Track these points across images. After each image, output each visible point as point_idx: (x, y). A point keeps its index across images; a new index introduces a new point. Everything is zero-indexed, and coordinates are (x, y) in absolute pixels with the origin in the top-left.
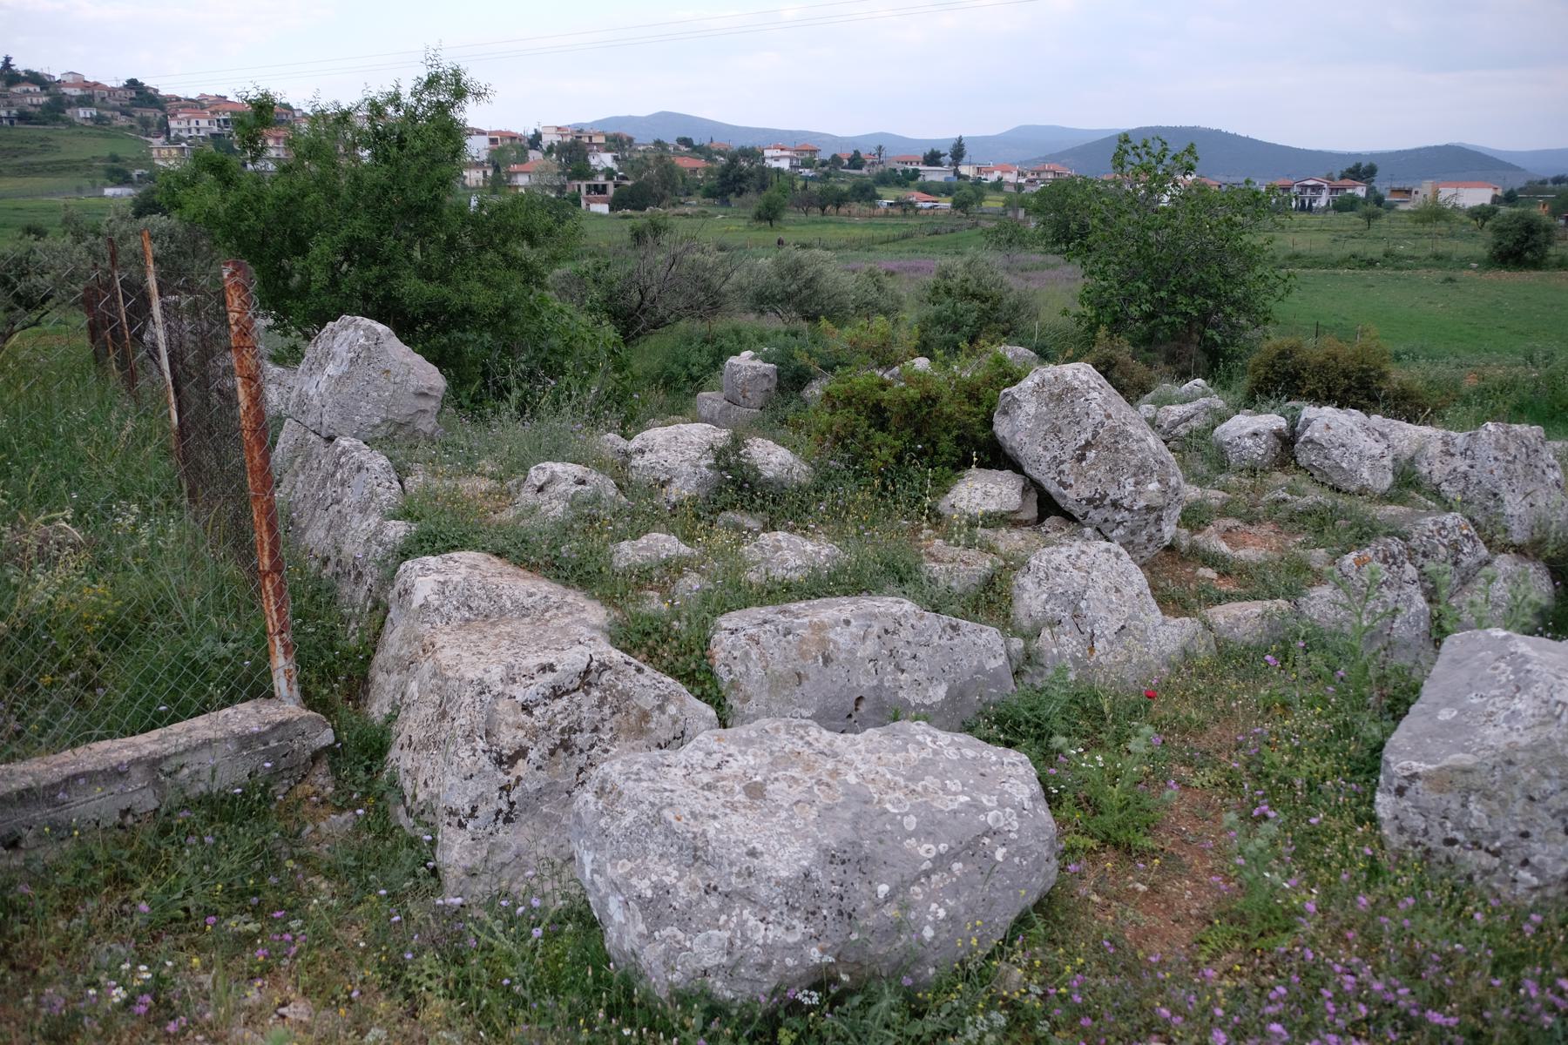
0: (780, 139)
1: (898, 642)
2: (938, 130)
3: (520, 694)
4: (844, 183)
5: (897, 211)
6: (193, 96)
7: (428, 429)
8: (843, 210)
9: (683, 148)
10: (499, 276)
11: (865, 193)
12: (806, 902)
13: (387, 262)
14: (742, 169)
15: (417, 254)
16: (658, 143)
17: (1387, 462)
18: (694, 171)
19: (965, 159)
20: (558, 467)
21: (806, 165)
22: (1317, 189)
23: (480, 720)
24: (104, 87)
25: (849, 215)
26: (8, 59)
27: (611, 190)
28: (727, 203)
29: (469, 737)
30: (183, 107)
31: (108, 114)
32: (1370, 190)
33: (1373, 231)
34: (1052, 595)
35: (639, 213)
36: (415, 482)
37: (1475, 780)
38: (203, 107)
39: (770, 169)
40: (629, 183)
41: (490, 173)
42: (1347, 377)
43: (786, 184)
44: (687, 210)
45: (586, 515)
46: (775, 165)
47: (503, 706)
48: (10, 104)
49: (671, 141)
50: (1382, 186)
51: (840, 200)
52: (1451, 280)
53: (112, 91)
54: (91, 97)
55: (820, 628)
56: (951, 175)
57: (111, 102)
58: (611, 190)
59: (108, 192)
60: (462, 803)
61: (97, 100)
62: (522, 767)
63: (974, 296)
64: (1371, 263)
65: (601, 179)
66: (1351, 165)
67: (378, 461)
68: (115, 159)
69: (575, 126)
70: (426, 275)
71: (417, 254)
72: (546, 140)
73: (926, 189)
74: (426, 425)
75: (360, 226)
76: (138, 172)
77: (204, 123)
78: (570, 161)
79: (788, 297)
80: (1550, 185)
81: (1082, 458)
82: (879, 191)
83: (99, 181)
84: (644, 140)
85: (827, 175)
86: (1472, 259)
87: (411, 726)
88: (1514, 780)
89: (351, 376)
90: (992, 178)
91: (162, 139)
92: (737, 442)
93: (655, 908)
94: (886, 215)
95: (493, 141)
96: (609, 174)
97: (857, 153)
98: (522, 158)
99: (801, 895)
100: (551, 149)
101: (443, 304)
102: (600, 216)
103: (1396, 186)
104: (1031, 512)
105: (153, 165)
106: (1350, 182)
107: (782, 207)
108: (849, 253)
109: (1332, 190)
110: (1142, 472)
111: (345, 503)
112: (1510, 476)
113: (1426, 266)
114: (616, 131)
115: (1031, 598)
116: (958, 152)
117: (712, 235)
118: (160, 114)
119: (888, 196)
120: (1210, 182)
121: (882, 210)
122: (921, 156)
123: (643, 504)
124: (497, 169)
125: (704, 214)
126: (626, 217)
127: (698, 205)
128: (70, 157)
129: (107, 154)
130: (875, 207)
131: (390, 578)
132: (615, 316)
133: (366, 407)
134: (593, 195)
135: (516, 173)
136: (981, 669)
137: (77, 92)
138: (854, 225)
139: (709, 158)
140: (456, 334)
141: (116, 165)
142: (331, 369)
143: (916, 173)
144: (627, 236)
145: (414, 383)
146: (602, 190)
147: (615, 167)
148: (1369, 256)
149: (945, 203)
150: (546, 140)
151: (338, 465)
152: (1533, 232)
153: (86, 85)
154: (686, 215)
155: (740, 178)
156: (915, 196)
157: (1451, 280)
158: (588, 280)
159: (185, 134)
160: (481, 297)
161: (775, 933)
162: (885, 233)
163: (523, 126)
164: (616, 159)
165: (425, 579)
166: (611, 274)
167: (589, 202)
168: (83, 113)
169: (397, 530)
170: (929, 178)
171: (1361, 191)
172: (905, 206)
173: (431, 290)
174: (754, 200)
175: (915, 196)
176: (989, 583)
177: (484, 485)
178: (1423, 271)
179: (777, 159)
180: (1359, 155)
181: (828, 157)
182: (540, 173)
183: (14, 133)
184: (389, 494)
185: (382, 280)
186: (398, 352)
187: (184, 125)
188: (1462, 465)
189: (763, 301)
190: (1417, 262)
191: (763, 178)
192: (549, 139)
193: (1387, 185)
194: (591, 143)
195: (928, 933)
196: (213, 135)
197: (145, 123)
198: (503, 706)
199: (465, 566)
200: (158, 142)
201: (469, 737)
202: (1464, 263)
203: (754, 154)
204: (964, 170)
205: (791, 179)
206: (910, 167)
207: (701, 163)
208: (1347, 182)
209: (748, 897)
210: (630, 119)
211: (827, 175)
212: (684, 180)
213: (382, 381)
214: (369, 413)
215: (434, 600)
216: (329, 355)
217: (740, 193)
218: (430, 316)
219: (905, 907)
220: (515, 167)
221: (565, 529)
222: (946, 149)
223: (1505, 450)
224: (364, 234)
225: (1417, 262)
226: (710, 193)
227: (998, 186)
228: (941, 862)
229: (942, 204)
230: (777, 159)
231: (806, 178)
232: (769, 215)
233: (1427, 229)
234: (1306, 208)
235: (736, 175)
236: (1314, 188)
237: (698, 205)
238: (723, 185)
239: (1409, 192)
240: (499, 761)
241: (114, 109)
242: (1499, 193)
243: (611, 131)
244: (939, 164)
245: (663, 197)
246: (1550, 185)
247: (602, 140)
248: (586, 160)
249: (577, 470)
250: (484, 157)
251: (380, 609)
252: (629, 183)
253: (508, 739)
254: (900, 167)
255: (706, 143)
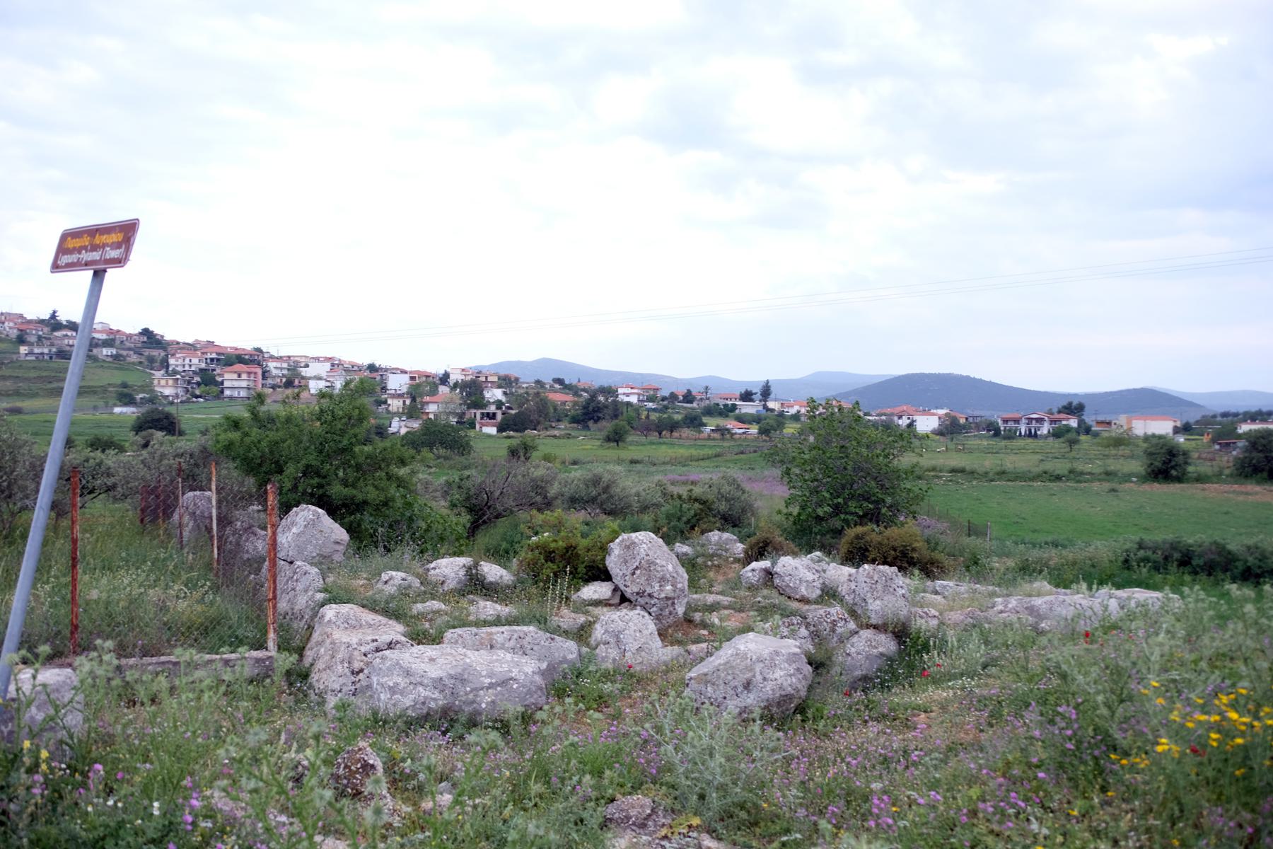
0: (630, 380)
1: (525, 642)
2: (753, 376)
3: (363, 649)
4: (677, 414)
5: (717, 435)
6: (190, 341)
7: (339, 559)
8: (675, 434)
9: (557, 386)
10: (383, 484)
11: (694, 422)
12: (440, 687)
13: (325, 477)
14: (599, 402)
15: (341, 474)
16: (538, 382)
17: (817, 584)
18: (564, 403)
19: (772, 396)
20: (394, 573)
21: (650, 399)
22: (1040, 420)
23: (347, 656)
24: (124, 334)
25: (680, 438)
26: (55, 312)
27: (499, 417)
28: (587, 428)
29: (342, 662)
30: (182, 348)
31: (124, 353)
32: (1081, 422)
33: (1073, 454)
34: (606, 631)
35: (519, 434)
36: (330, 579)
37: (709, 678)
38: (196, 349)
39: (622, 403)
40: (513, 412)
41: (408, 402)
42: (895, 550)
43: (633, 414)
44: (556, 432)
45: (404, 591)
46: (626, 399)
47: (356, 653)
48: (52, 345)
49: (547, 380)
50: (1089, 419)
51: (673, 427)
52: (1113, 490)
53: (130, 336)
54: (113, 340)
55: (491, 634)
56: (761, 408)
57: (128, 344)
58: (499, 417)
59: (117, 410)
60: (337, 687)
61: (118, 342)
62: (361, 676)
63: (696, 500)
64: (1058, 478)
65: (492, 409)
66: (1065, 403)
67: (314, 570)
68: (125, 385)
69: (476, 367)
70: (345, 484)
71: (341, 474)
72: (453, 378)
73: (741, 419)
74: (338, 557)
75: (312, 459)
76: (141, 396)
77: (195, 361)
78: (469, 395)
79: (593, 500)
80: (1219, 419)
81: (633, 574)
82: (705, 420)
83: (111, 403)
84: (527, 379)
85: (666, 408)
86: (1130, 475)
87: (320, 665)
88: (719, 677)
89: (309, 529)
90: (793, 411)
91: (162, 372)
92: (476, 565)
93: (393, 690)
94: (709, 438)
95: (412, 378)
96: (499, 404)
97: (689, 391)
98: (434, 392)
99: (438, 684)
100: (456, 385)
101: (353, 498)
102: (490, 436)
103: (1100, 418)
104: (617, 600)
105: (153, 391)
106: (1065, 416)
107: (626, 432)
108: (668, 467)
109: (1052, 422)
110: (663, 580)
111: (300, 587)
112: (872, 590)
113: (1099, 480)
114: (507, 373)
115: (598, 633)
116: (766, 392)
117: (571, 456)
118: (163, 354)
119: (711, 424)
120: (959, 415)
121: (705, 435)
122: (738, 394)
123: (431, 590)
124: (414, 399)
125: (568, 436)
126: (509, 437)
127: (566, 428)
128: (91, 384)
129: (119, 382)
130: (701, 432)
131: (315, 614)
132: (471, 510)
133: (310, 548)
134: (486, 420)
135: (428, 403)
136: (564, 657)
137: (104, 337)
138: (681, 446)
139: (576, 394)
140: (358, 515)
141: (125, 390)
142: (294, 530)
143: (734, 407)
144: (504, 452)
145: (334, 537)
146: (492, 416)
147: (504, 399)
148: (1057, 472)
149: (754, 430)
150: (453, 378)
151: (295, 573)
152: (1174, 456)
153: (111, 332)
154: (555, 436)
155: (598, 409)
156: (730, 424)
157: (1113, 490)
158: (455, 486)
159: (180, 369)
160: (372, 494)
161: (427, 693)
162: (702, 452)
163: (437, 369)
164: (505, 393)
165: (330, 612)
166: (467, 484)
167: (482, 425)
168: (106, 351)
169: (320, 596)
170: (744, 411)
171: (1073, 423)
172: (722, 431)
173: (347, 491)
174: (607, 426)
175: (730, 424)
176: (582, 628)
177: (361, 583)
178: (1097, 484)
179: (628, 395)
180: (1069, 395)
181: (667, 395)
182: (447, 403)
183: (52, 365)
184: (319, 583)
185: (320, 486)
186: (327, 521)
187: (180, 361)
188: (853, 586)
189: (575, 502)
190: (1093, 477)
191: (616, 410)
192: (455, 377)
193: (1093, 418)
194: (487, 381)
195: (484, 706)
196: (201, 370)
197: (151, 360)
198: (356, 653)
199: (346, 609)
200: (159, 374)
201: (342, 662)
202: (1127, 478)
203: (610, 391)
204: (771, 405)
205: (637, 409)
206: (729, 402)
207: (569, 398)
208: (1063, 416)
209: (421, 684)
210: (519, 363)
211: (666, 408)
212: (555, 409)
213: (319, 536)
214: (311, 550)
215: (334, 619)
216: (293, 523)
217: (597, 420)
218: (344, 505)
219: (476, 696)
220: (427, 399)
221: (392, 597)
222: (757, 390)
223: (872, 578)
224: (313, 463)
225: (1093, 477)
226: (575, 420)
227: (796, 417)
228: (491, 686)
229: (751, 431)
230: (628, 395)
231: (649, 410)
232: (616, 438)
233: (1113, 452)
234: (1032, 435)
235: (596, 409)
236: (1038, 420)
237: (566, 428)
238: (585, 414)
239: (1109, 423)
240: (353, 673)
241: (129, 349)
242: (1178, 424)
243: (503, 373)
244: (752, 400)
245: (539, 423)
246: (1219, 419)
247: (495, 379)
248: (481, 393)
249: (402, 575)
250: (404, 390)
251: (310, 628)
252: (513, 412)
253: (357, 665)
254: (722, 402)
255: (574, 382)
